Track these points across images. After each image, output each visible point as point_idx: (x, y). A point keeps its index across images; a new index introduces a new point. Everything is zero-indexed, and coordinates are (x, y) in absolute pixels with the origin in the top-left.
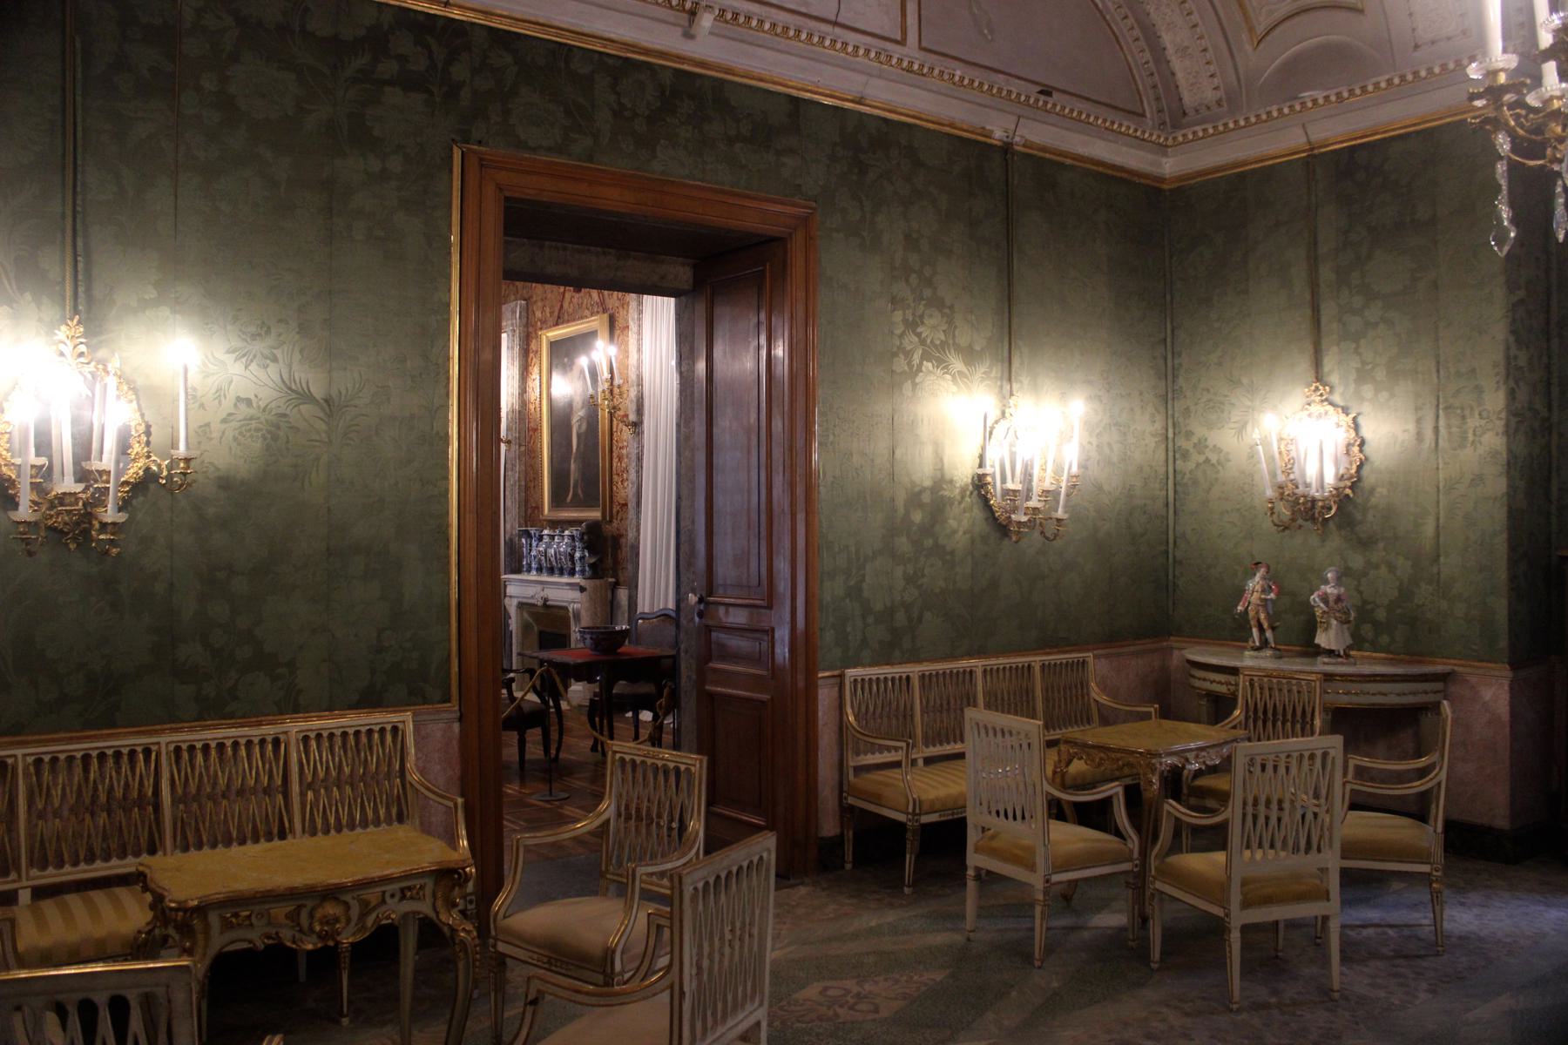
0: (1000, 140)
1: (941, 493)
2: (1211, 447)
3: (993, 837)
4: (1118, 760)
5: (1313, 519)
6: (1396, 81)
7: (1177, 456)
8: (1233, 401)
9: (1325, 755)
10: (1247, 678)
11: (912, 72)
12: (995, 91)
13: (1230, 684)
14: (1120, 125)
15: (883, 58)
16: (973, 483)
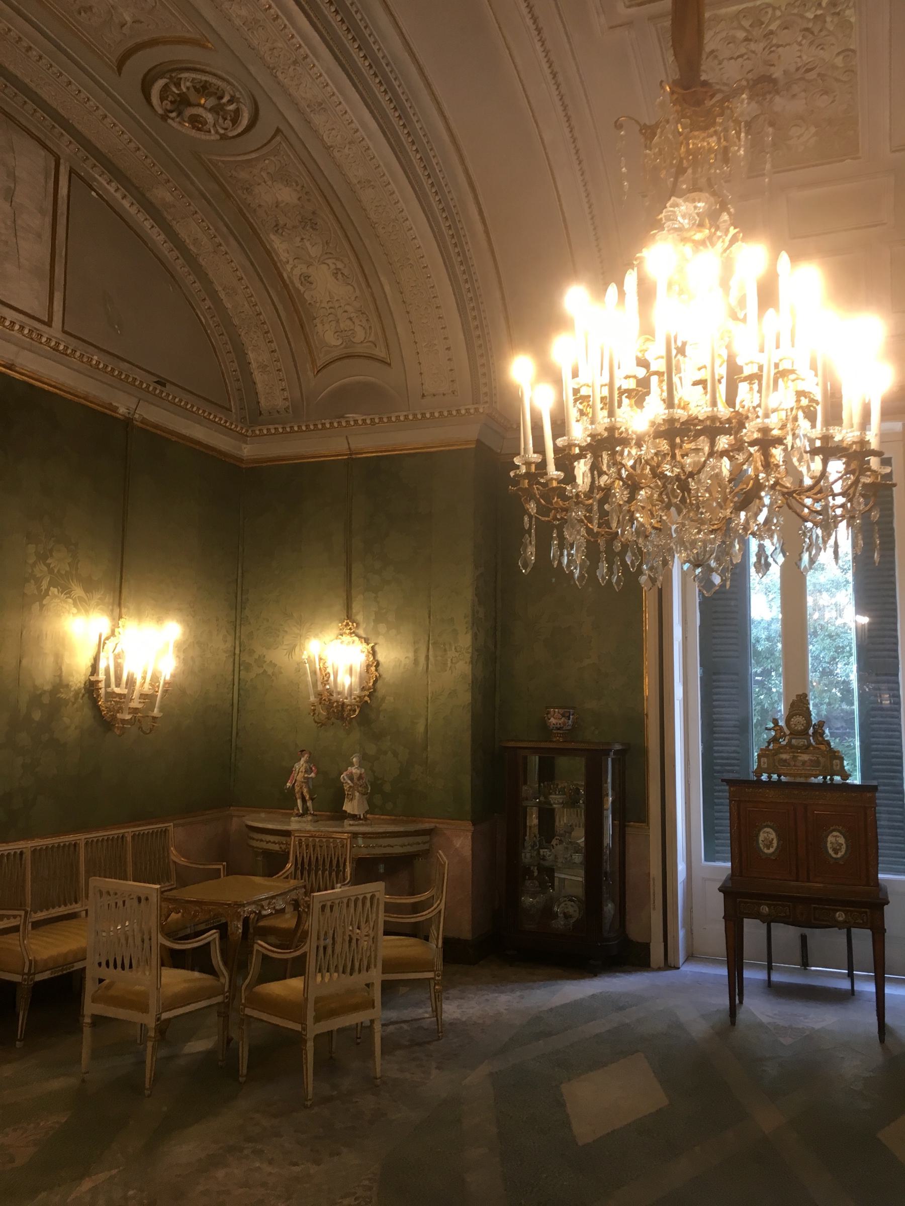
0: (122, 415)
1: (58, 695)
2: (268, 662)
3: (109, 987)
4: (210, 911)
5: (342, 718)
6: (411, 417)
7: (242, 668)
8: (286, 629)
9: (372, 897)
10: (297, 839)
11: (57, 350)
12: (123, 377)
13: (283, 844)
14: (215, 417)
15: (34, 335)
16: (85, 688)
